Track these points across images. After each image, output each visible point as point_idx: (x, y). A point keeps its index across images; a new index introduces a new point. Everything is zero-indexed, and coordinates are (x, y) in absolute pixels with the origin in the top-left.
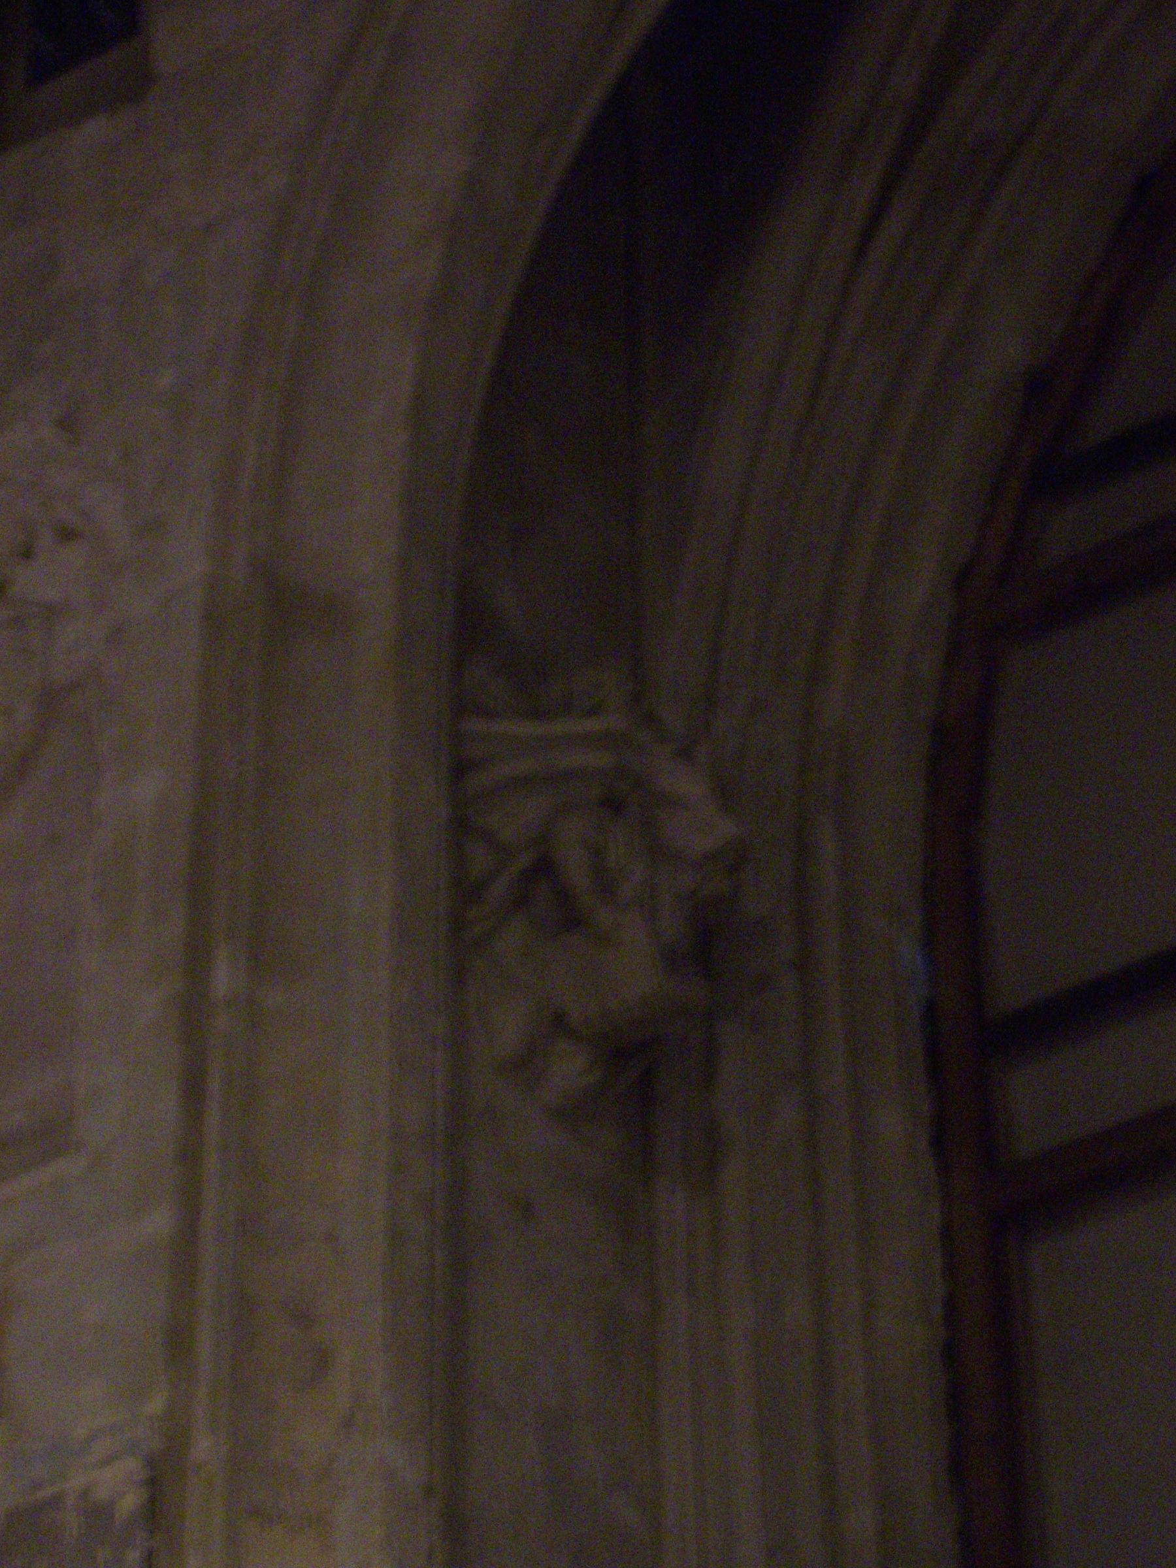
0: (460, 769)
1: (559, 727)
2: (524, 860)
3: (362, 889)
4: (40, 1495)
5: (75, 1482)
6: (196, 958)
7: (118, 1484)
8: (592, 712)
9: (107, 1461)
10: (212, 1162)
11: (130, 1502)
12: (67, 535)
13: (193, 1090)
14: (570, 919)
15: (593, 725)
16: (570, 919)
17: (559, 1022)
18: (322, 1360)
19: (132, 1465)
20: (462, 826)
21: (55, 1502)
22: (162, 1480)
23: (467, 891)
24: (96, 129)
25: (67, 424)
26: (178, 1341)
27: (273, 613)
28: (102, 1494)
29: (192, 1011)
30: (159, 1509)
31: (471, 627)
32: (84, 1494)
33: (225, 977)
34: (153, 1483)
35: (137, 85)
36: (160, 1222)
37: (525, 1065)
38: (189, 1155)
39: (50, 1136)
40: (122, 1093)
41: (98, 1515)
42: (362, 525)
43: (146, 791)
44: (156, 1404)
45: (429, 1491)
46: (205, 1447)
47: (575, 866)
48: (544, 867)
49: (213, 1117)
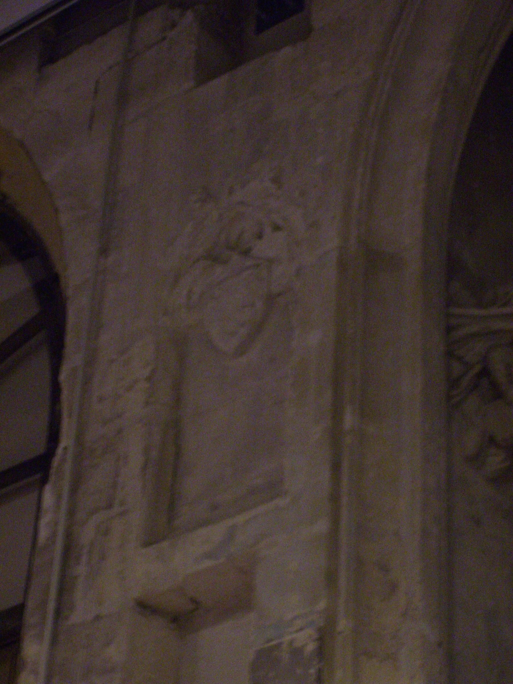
0: (449, 329)
1: (494, 311)
2: (477, 368)
3: (409, 380)
4: (271, 644)
5: (287, 638)
6: (337, 414)
7: (305, 639)
8: (505, 305)
9: (301, 629)
10: (344, 500)
11: (311, 647)
12: (277, 228)
13: (336, 468)
14: (497, 394)
15: (506, 310)
16: (497, 394)
17: (492, 441)
18: (393, 587)
19: (310, 632)
20: (449, 354)
21: (279, 645)
22: (325, 637)
23: (453, 383)
24: (287, 51)
25: (276, 181)
26: (331, 578)
27: (367, 264)
28: (298, 644)
29: (335, 436)
30: (322, 652)
31: (453, 267)
32: (291, 642)
33: (349, 420)
34: (321, 640)
35: (305, 33)
36: (322, 526)
37: (476, 459)
38: (335, 498)
39: (273, 488)
40: (305, 470)
41: (297, 652)
42: (406, 222)
43: (314, 339)
44: (322, 605)
45: (440, 645)
46: (343, 624)
47: (500, 373)
48: (485, 372)
49: (345, 482)
